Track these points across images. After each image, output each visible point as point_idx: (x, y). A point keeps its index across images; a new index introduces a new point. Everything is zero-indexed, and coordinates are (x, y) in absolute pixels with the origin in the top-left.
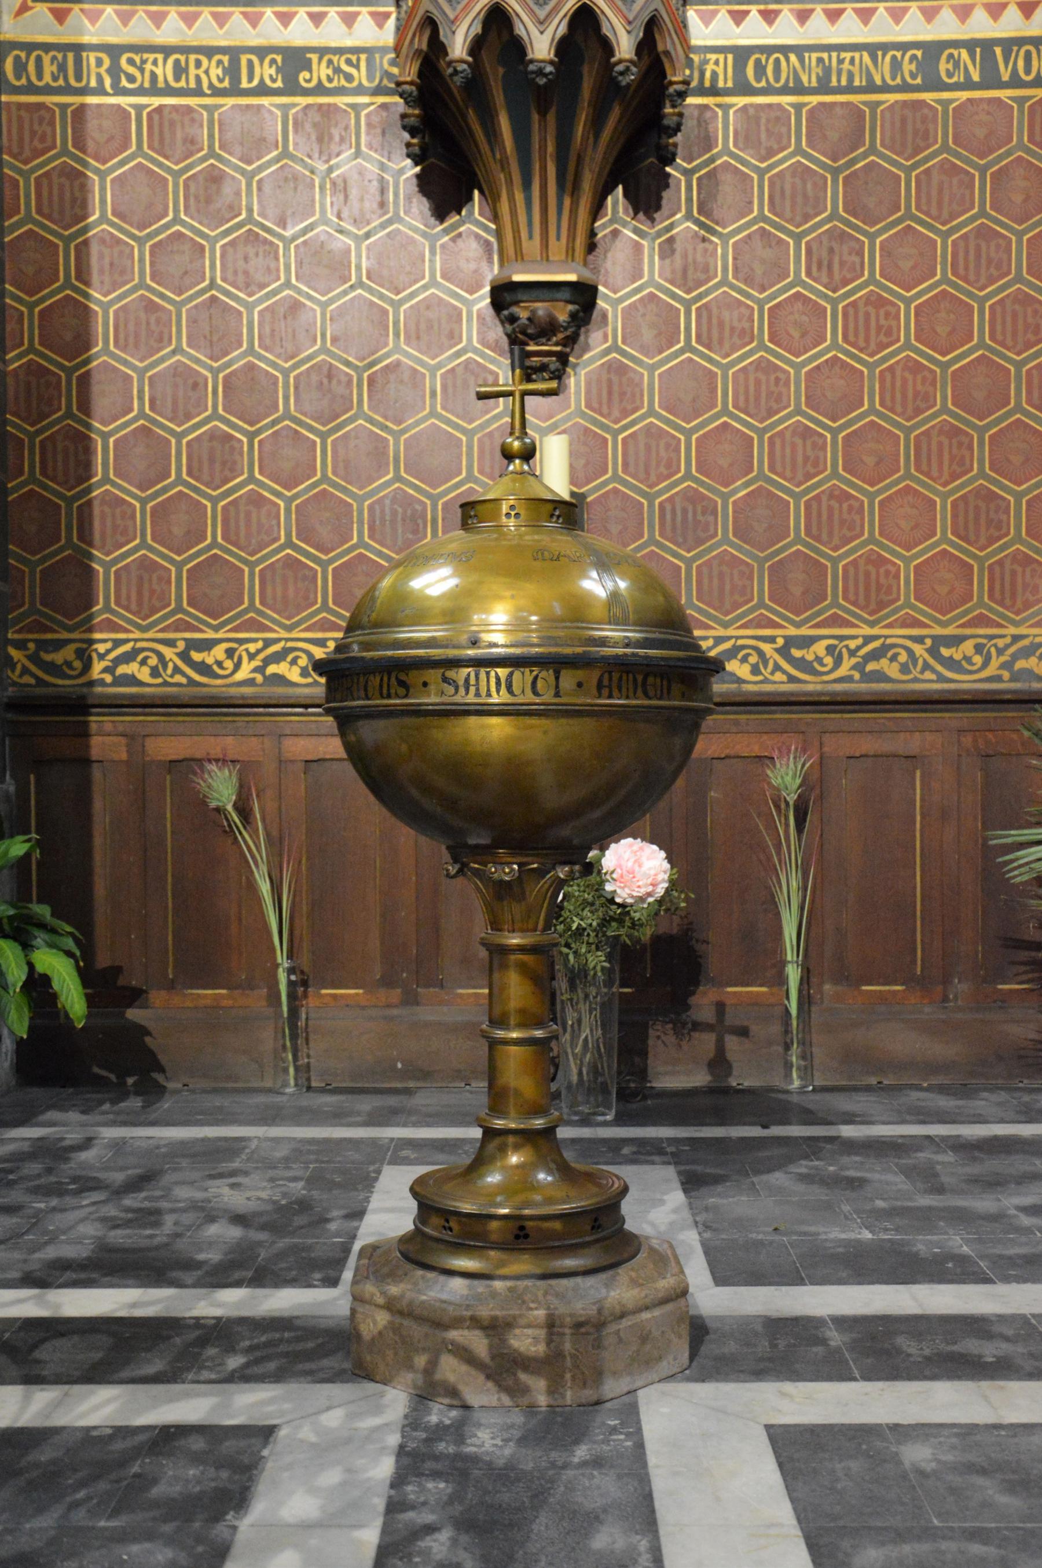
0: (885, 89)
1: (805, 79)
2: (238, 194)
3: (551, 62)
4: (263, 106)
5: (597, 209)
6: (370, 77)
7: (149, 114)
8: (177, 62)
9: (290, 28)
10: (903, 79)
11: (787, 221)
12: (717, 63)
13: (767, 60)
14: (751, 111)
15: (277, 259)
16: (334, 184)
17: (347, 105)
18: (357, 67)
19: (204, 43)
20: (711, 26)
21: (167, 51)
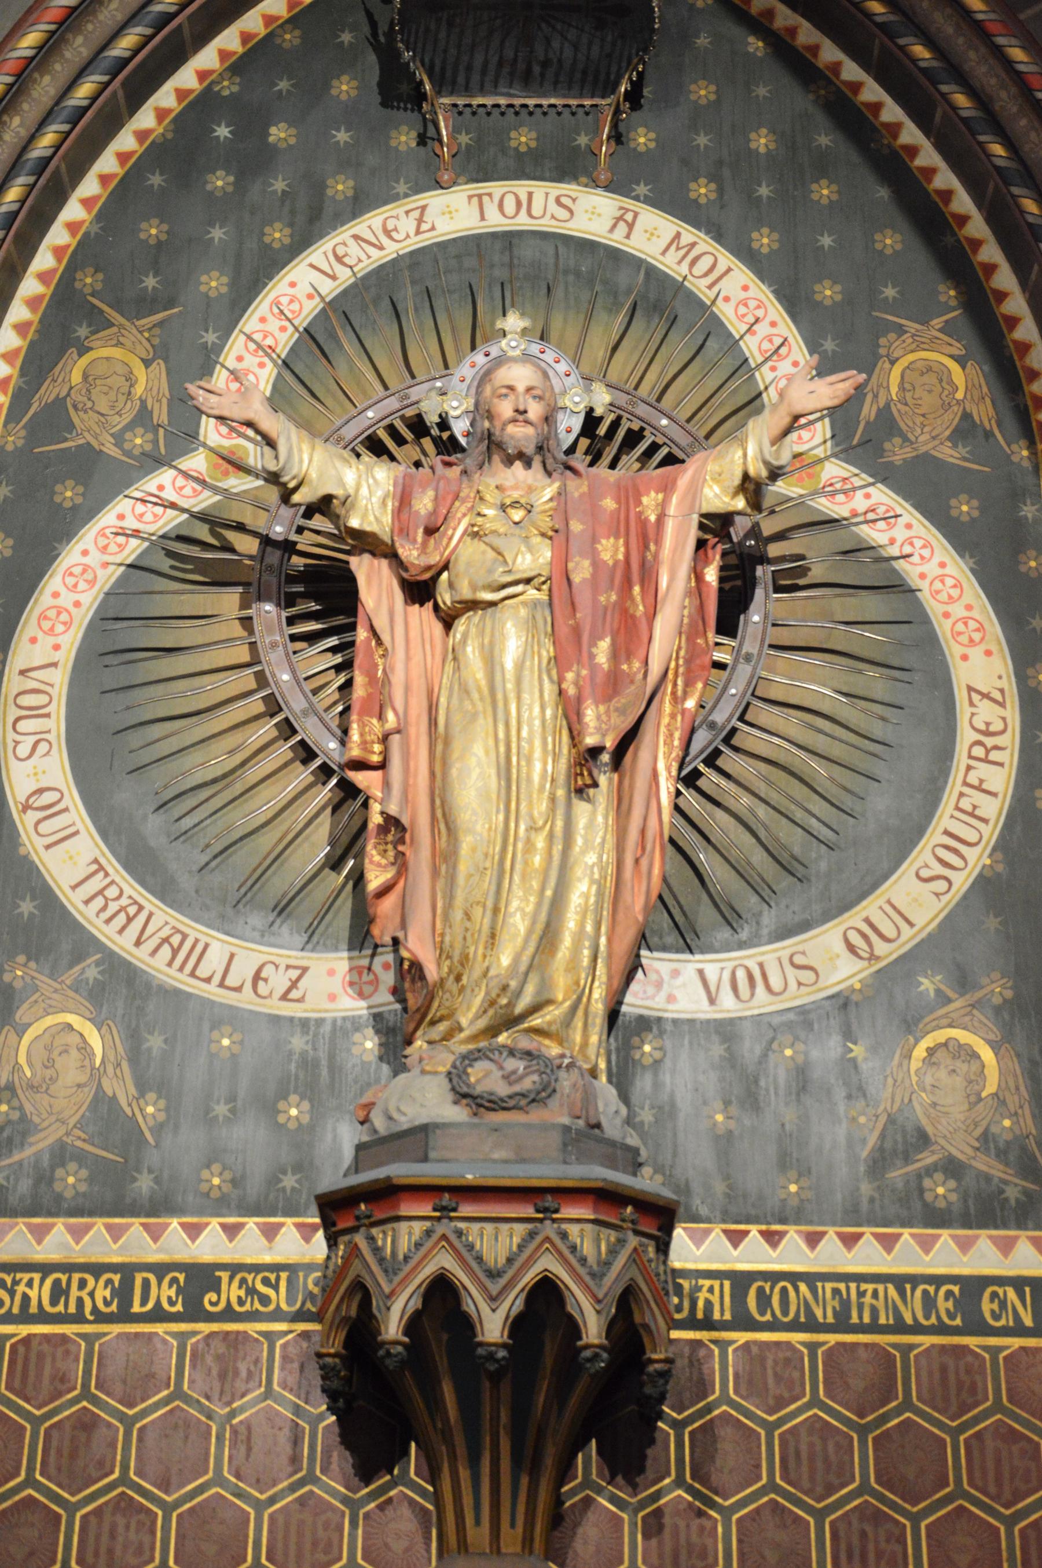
0: (917, 1329)
1: (819, 1313)
2: (113, 1445)
3: (504, 1346)
4: (156, 1334)
5: (565, 1471)
6: (290, 1301)
7: (13, 1346)
8: (57, 1283)
9: (198, 1242)
10: (938, 1317)
11: (806, 1493)
12: (711, 1290)
13: (772, 1289)
14: (755, 1350)
15: (153, 1533)
16: (235, 1431)
17: (259, 1333)
18: (276, 1288)
19: (93, 1260)
20: (703, 1248)
21: (46, 1269)
